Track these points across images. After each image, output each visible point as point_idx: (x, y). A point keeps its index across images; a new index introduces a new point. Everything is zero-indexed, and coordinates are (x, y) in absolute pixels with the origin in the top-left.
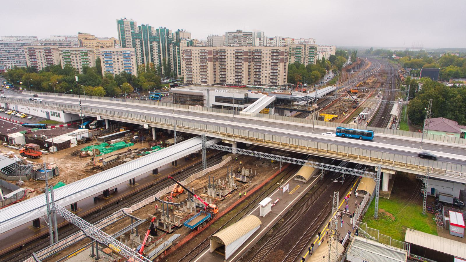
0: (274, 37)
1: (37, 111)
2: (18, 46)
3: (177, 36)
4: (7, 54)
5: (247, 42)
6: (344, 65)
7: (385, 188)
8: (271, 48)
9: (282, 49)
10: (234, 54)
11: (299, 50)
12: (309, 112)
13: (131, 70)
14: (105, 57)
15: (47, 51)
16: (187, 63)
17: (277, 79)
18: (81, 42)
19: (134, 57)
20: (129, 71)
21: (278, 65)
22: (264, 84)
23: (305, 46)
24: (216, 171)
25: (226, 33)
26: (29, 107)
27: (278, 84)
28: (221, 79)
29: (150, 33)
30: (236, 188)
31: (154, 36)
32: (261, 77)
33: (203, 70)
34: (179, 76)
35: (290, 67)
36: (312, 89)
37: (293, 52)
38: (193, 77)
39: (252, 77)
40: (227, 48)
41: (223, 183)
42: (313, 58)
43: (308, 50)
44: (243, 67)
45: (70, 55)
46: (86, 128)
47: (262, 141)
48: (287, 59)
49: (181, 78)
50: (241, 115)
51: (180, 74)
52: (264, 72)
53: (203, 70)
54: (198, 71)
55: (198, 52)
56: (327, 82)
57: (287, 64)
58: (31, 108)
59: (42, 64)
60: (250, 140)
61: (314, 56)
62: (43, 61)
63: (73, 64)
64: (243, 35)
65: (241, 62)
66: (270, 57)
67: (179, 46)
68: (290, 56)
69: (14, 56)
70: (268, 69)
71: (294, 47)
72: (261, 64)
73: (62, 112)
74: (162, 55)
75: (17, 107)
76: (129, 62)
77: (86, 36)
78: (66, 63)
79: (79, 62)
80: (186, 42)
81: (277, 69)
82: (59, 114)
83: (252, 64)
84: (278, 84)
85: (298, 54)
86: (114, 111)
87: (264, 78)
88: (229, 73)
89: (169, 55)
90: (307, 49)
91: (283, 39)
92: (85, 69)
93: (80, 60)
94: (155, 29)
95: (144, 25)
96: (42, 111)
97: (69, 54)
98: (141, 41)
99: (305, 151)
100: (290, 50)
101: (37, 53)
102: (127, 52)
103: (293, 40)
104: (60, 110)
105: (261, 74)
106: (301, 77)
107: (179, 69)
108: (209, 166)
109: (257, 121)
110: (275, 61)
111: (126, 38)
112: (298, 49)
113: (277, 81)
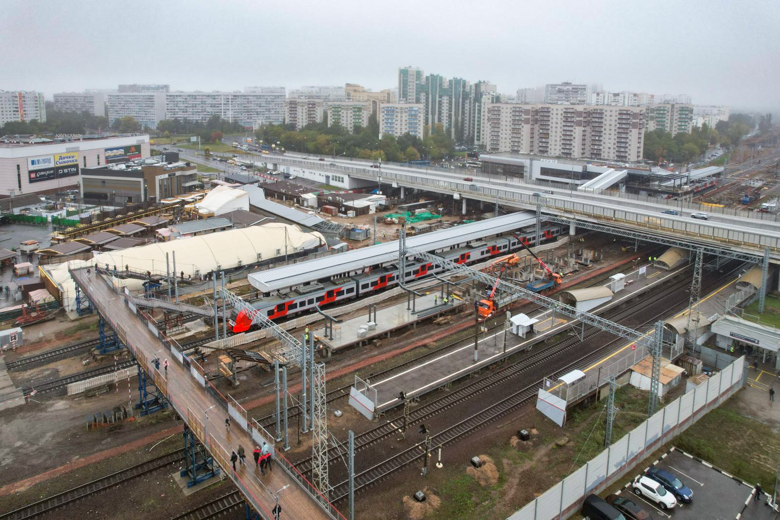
0: (621, 92)
1: (314, 174)
2: (272, 99)
5: (578, 98)
6: (744, 138)
9: (637, 110)
10: (562, 114)
11: (662, 112)
13: (416, 131)
15: (311, 106)
16: (493, 125)
17: (627, 147)
18: (349, 95)
20: (413, 133)
21: (628, 131)
22: (606, 158)
23: (673, 106)
25: (547, 86)
26: (304, 170)
27: (629, 159)
29: (441, 85)
30: (578, 269)
31: (445, 89)
33: (515, 135)
34: (476, 142)
35: (648, 136)
39: (588, 148)
40: (552, 106)
42: (687, 124)
45: (340, 111)
46: (383, 194)
48: (643, 124)
49: (479, 145)
50: (580, 191)
51: (478, 140)
52: (607, 141)
53: (515, 135)
54: (508, 137)
55: (509, 111)
56: (709, 160)
57: (643, 131)
58: (307, 171)
61: (687, 122)
62: (304, 117)
63: (342, 122)
64: (573, 88)
65: (572, 126)
66: (616, 120)
67: (480, 103)
68: (647, 121)
71: (653, 107)
73: (347, 176)
75: (288, 169)
76: (415, 121)
77: (356, 88)
78: (334, 121)
79: (349, 119)
80: (490, 97)
81: (627, 138)
82: (343, 178)
83: (588, 129)
84: (629, 159)
87: (606, 150)
88: (553, 141)
89: (463, 113)
90: (675, 110)
91: (635, 95)
92: (357, 128)
93: (351, 117)
96: (320, 175)
97: (339, 109)
98: (427, 94)
100: (647, 111)
101: (299, 107)
103: (652, 96)
104: (345, 174)
105: (602, 143)
106: (665, 151)
110: (624, 126)
111: (409, 91)
112: (661, 110)
113: (627, 155)
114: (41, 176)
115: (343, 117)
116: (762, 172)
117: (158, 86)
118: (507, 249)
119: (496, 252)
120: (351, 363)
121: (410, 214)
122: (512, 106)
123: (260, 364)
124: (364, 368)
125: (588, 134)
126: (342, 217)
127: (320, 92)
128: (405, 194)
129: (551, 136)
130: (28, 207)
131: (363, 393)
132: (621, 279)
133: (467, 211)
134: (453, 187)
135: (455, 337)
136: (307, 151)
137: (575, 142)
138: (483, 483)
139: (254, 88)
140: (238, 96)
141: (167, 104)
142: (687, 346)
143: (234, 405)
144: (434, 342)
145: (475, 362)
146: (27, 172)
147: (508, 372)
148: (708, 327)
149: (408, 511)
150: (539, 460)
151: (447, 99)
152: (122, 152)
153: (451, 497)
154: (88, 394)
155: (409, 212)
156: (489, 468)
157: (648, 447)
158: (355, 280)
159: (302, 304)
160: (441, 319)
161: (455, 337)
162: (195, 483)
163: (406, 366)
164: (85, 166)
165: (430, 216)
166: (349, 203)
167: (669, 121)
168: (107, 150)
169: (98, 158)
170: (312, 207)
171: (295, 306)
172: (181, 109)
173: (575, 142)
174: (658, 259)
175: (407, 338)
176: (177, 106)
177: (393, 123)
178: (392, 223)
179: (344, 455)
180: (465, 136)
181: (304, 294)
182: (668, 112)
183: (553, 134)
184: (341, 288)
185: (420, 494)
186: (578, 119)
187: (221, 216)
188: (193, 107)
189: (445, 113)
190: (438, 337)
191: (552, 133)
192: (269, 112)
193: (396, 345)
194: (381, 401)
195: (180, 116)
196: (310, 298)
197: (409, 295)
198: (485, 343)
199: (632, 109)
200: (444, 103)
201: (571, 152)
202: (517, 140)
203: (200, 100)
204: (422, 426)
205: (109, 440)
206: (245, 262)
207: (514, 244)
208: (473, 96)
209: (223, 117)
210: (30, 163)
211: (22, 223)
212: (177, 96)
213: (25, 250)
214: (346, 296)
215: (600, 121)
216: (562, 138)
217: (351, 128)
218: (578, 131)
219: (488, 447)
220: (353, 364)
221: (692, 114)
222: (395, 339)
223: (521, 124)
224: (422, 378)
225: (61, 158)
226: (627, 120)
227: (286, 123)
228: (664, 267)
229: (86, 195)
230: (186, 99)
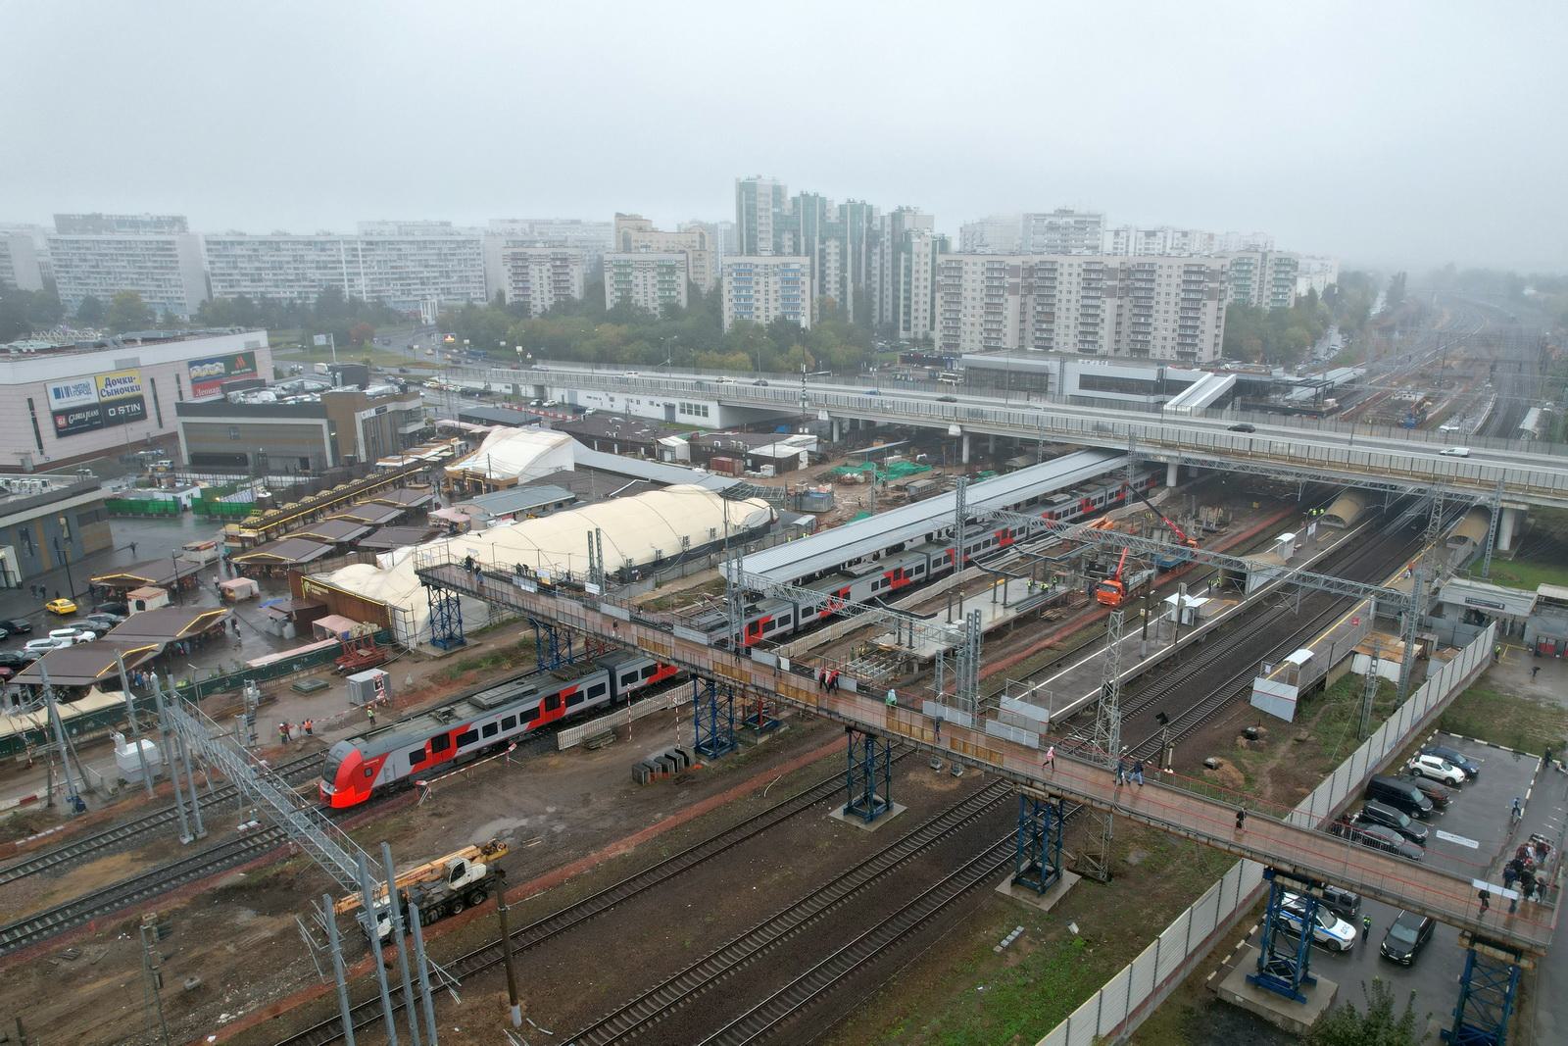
2: (450, 249)
3: (893, 225)
4: (422, 269)
7: (1505, 544)
8: (1182, 262)
9: (1216, 265)
11: (1245, 268)
14: (735, 279)
17: (1196, 345)
19: (807, 279)
23: (1264, 256)
26: (611, 395)
27: (1200, 358)
32: (1150, 338)
33: (991, 318)
34: (902, 334)
39: (1125, 340)
44: (1104, 311)
45: (630, 274)
46: (810, 434)
51: (907, 329)
52: (1159, 324)
53: (991, 318)
54: (978, 320)
55: (979, 269)
59: (542, 298)
62: (546, 288)
63: (636, 297)
64: (1076, 222)
65: (1099, 298)
67: (909, 252)
69: (437, 274)
70: (1172, 316)
72: (1153, 303)
74: (849, 275)
75: (573, 395)
77: (640, 224)
79: (650, 289)
80: (930, 241)
81: (1198, 318)
82: (705, 408)
87: (1159, 343)
90: (1268, 265)
92: (671, 310)
94: (836, 206)
95: (807, 195)
97: (629, 270)
101: (532, 266)
102: (792, 267)
104: (711, 398)
107: (905, 314)
111: (760, 228)
112: (1244, 264)
113: (1196, 350)
115: (637, 285)
117: (158, 217)
118: (923, 575)
119: (902, 582)
122: (984, 259)
127: (532, 232)
129: (1059, 317)
131: (1023, 699)
133: (971, 457)
134: (948, 415)
136: (578, 358)
139: (379, 223)
140: (377, 243)
141: (211, 262)
145: (1142, 658)
146: (49, 414)
150: (1284, 757)
151: (836, 247)
154: (587, 746)
158: (603, 666)
159: (490, 730)
161: (1084, 634)
164: (181, 398)
167: (1256, 286)
168: (192, 364)
169: (178, 381)
171: (473, 736)
174: (1327, 513)
176: (235, 268)
177: (751, 297)
181: (491, 707)
183: (1063, 314)
184: (576, 687)
186: (1110, 283)
188: (273, 268)
189: (833, 276)
191: (1061, 313)
192: (448, 277)
194: (1054, 710)
195: (246, 287)
196: (506, 715)
199: (1207, 262)
202: (995, 326)
205: (686, 792)
206: (667, 553)
207: (937, 563)
208: (886, 239)
209: (347, 290)
210: (52, 395)
211: (119, 514)
212: (232, 243)
214: (587, 703)
215: (1149, 286)
216: (1080, 320)
218: (1108, 307)
221: (1296, 270)
223: (1002, 296)
225: (109, 383)
226: (1198, 281)
227: (508, 301)
228: (1337, 525)
230: (255, 250)
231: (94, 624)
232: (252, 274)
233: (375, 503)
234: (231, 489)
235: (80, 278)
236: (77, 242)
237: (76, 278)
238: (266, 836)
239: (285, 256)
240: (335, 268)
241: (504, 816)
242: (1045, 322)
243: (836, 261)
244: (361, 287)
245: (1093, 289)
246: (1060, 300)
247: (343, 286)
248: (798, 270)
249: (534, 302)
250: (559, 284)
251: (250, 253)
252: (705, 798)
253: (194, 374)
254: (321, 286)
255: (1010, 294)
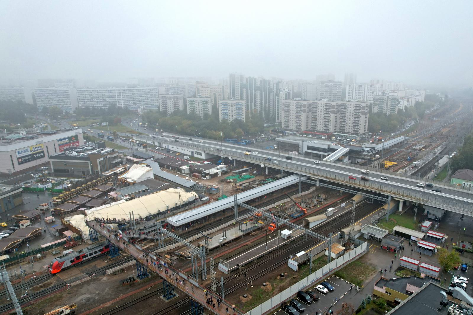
2: (148, 91)
4: (139, 97)
5: (337, 90)
10: (324, 107)
11: (382, 101)
12: (372, 161)
16: (286, 113)
17: (359, 126)
21: (360, 117)
22: (348, 131)
23: (388, 97)
24: (306, 195)
26: (178, 147)
27: (359, 132)
28: (312, 127)
29: (255, 83)
34: (277, 121)
36: (388, 138)
37: (377, 102)
38: (290, 124)
41: (310, 201)
42: (395, 107)
43: (390, 101)
44: (331, 118)
45: (194, 104)
46: (224, 165)
47: (334, 179)
49: (278, 123)
51: (278, 119)
52: (348, 122)
59: (171, 109)
60: (327, 178)
62: (172, 106)
67: (279, 96)
69: (144, 99)
70: (351, 120)
72: (346, 115)
74: (263, 101)
75: (168, 146)
79: (200, 108)
80: (285, 93)
82: (201, 153)
85: (381, 104)
86: (240, 154)
87: (348, 127)
88: (319, 122)
90: (389, 100)
92: (206, 115)
96: (188, 151)
97: (194, 103)
99: (358, 186)
101: (168, 100)
104: (202, 151)
105: (345, 123)
108: (303, 191)
109: (334, 166)
112: (381, 100)
113: (358, 130)
114: (24, 160)
115: (196, 107)
116: (427, 138)
120: (217, 254)
121: (239, 176)
123: (181, 257)
124: (223, 256)
125: (338, 118)
126: (204, 179)
128: (236, 164)
130: (27, 181)
131: (223, 265)
132: (332, 210)
135: (259, 240)
137: (330, 123)
138: (266, 291)
142: (350, 239)
143: (181, 272)
144: (251, 243)
146: (16, 159)
147: (278, 254)
148: (360, 230)
149: (241, 301)
151: (259, 93)
152: (67, 141)
153: (256, 295)
154: (114, 274)
155: (238, 175)
156: (269, 286)
157: (324, 276)
160: (253, 233)
161: (259, 240)
162: (169, 299)
163: (239, 254)
165: (249, 177)
166: (207, 171)
167: (385, 106)
168: (59, 140)
169: (55, 146)
170: (187, 174)
172: (89, 100)
173: (330, 123)
175: (239, 242)
176: (86, 98)
178: (230, 182)
179: (220, 285)
180: (271, 115)
182: (385, 101)
185: (245, 295)
186: (332, 110)
187: (142, 183)
188: (97, 98)
189: (258, 107)
190: (252, 241)
193: (234, 246)
194: (230, 267)
195: (89, 103)
197: (239, 223)
198: (271, 243)
200: (257, 95)
201: (329, 128)
202: (299, 122)
203: (101, 93)
204: (245, 274)
205: (131, 288)
209: (117, 104)
210: (17, 153)
211: (29, 191)
212: (85, 90)
213: (43, 209)
217: (202, 114)
218: (332, 117)
219: (269, 280)
220: (218, 255)
222: (234, 243)
223: (301, 113)
224: (246, 258)
225: (34, 148)
229: (55, 171)
230: (91, 93)
231: (9, 231)
232: (91, 100)
233: (94, 190)
234: (60, 183)
235: (43, 100)
236: (42, 90)
237: (42, 100)
238: (27, 299)
239: (100, 94)
240: (114, 98)
241: (85, 294)
242: (314, 120)
243: (259, 97)
244: (122, 103)
245: (328, 111)
246: (318, 114)
247: (116, 103)
248: (241, 105)
249: (168, 110)
250: (176, 105)
251: (90, 93)
252: (136, 290)
253: (59, 143)
254: (110, 103)
255: (303, 112)
